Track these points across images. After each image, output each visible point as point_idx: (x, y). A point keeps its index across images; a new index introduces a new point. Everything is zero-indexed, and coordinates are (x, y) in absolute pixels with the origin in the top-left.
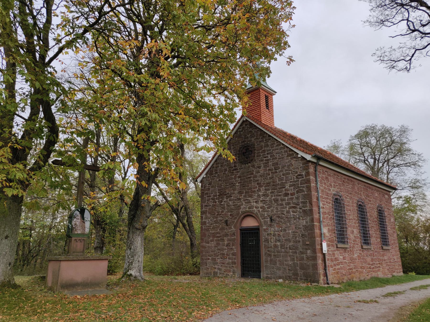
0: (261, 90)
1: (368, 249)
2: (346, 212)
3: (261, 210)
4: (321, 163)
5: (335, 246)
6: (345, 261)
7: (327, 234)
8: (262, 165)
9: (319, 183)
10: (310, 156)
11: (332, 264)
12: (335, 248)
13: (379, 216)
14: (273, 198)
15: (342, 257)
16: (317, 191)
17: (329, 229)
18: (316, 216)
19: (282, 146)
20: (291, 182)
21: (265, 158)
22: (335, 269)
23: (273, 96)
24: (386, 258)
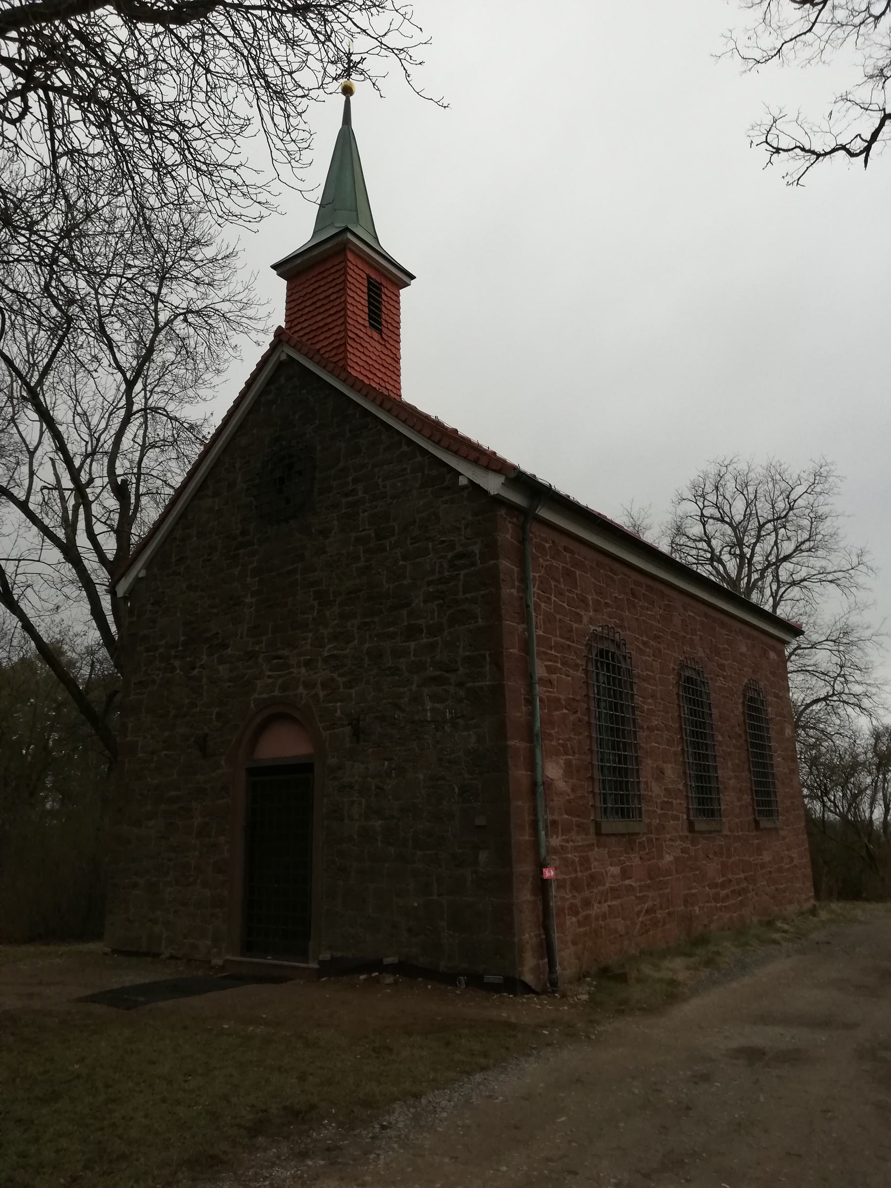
0: (350, 256)
1: (710, 832)
2: (638, 700)
3: (322, 694)
4: (544, 513)
5: (592, 830)
6: (627, 882)
7: (561, 785)
8: (336, 522)
9: (534, 589)
10: (501, 479)
11: (577, 902)
12: (592, 838)
13: (751, 717)
14: (367, 645)
15: (615, 870)
16: (525, 618)
17: (568, 764)
18: (516, 714)
19: (405, 448)
20: (429, 583)
21: (346, 495)
22: (587, 917)
23: (402, 292)
24: (767, 857)
